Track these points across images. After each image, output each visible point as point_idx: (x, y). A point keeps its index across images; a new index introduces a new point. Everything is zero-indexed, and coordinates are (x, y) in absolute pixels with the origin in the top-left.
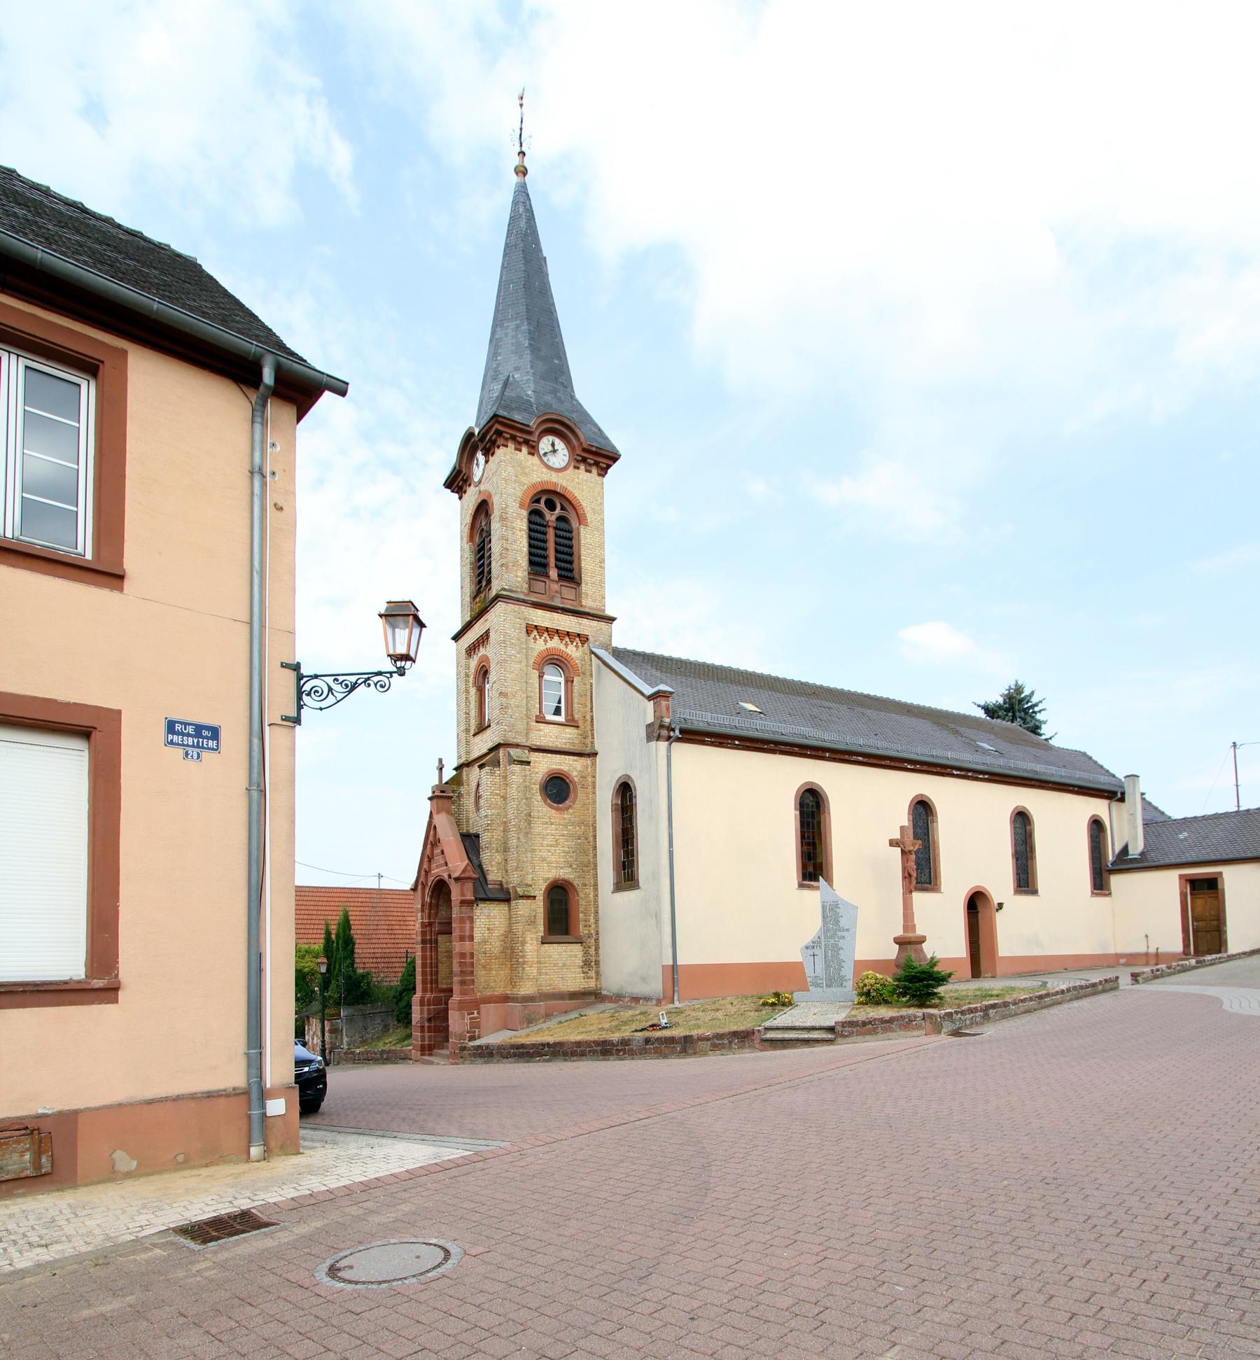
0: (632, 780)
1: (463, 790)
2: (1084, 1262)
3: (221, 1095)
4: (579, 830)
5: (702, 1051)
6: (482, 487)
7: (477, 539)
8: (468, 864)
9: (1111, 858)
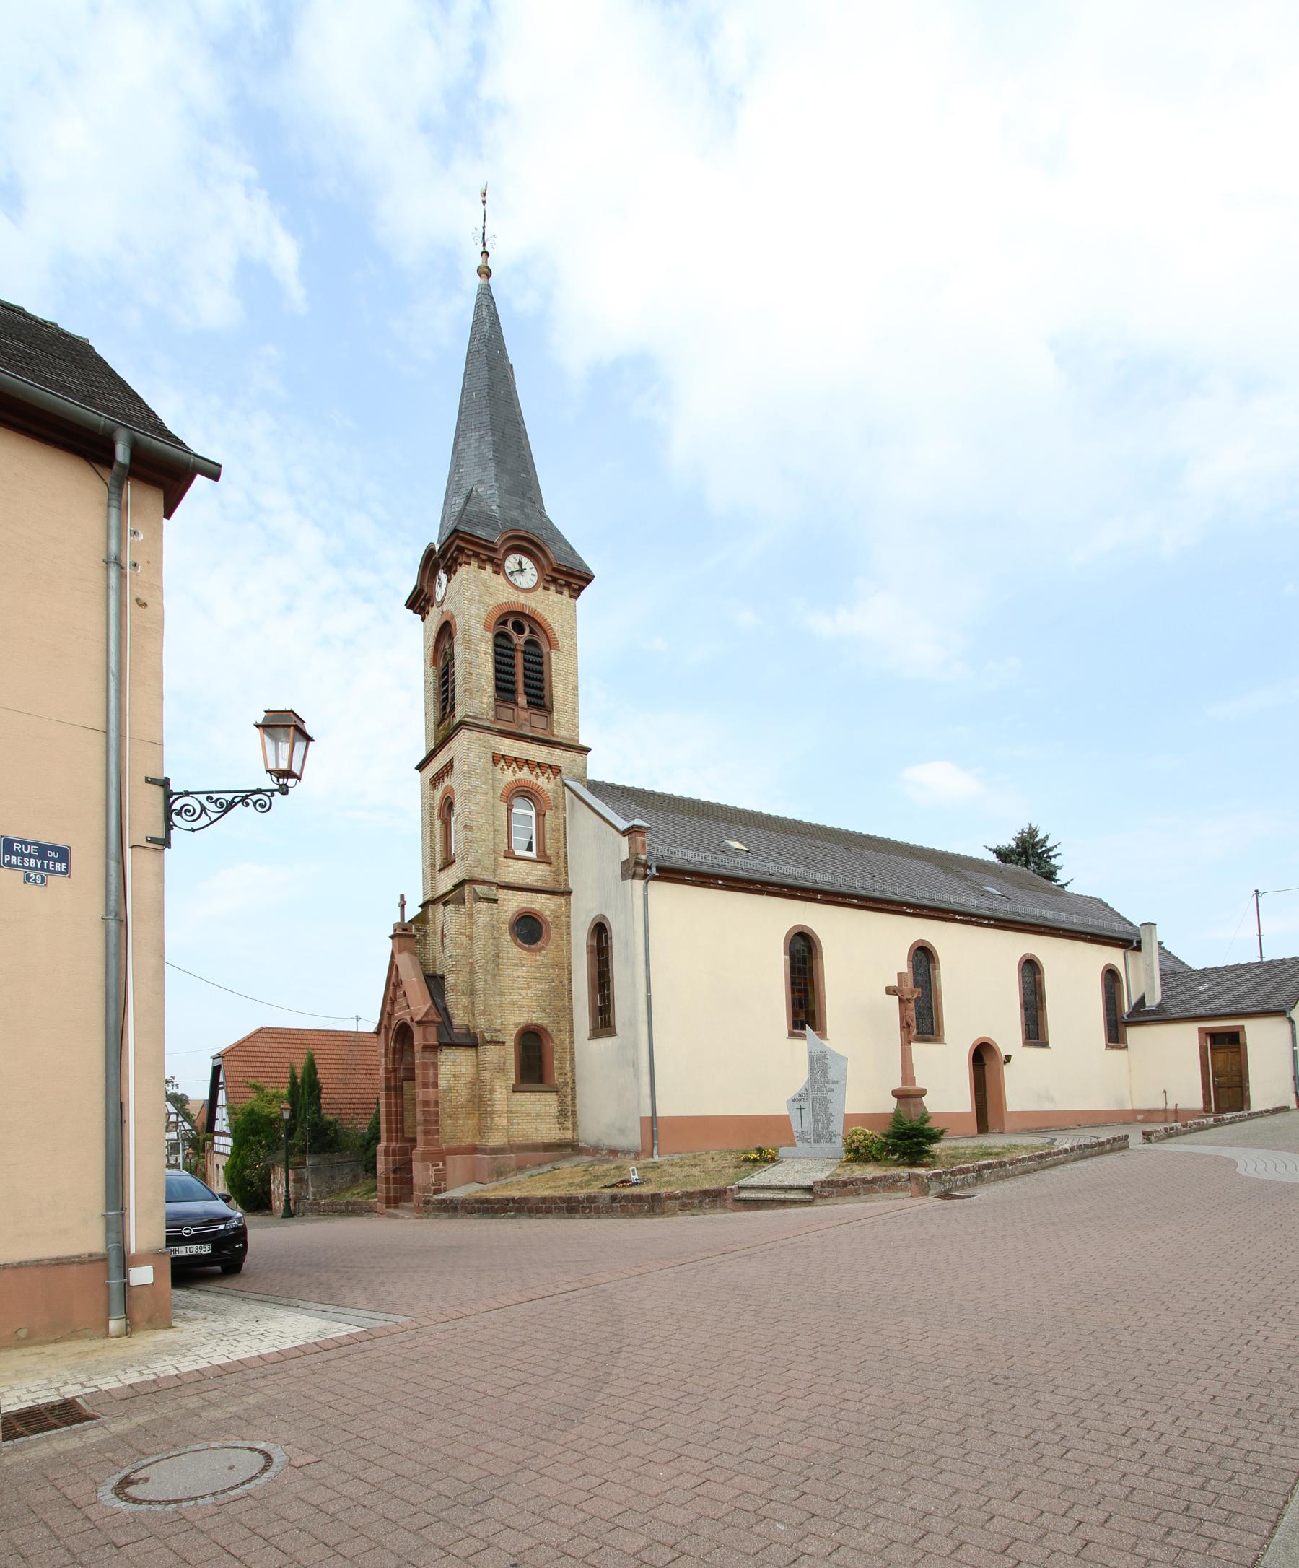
1: (429, 929)
2: (1013, 1494)
3: (74, 1262)
5: (670, 1210)
6: (445, 608)
7: (441, 663)
8: (430, 1008)
9: (1126, 1010)
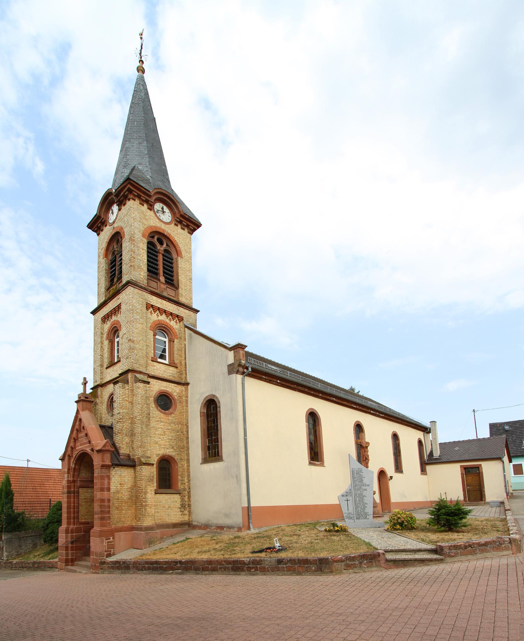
0: (217, 397)
4: (178, 427)
6: (115, 225)
7: (110, 257)
